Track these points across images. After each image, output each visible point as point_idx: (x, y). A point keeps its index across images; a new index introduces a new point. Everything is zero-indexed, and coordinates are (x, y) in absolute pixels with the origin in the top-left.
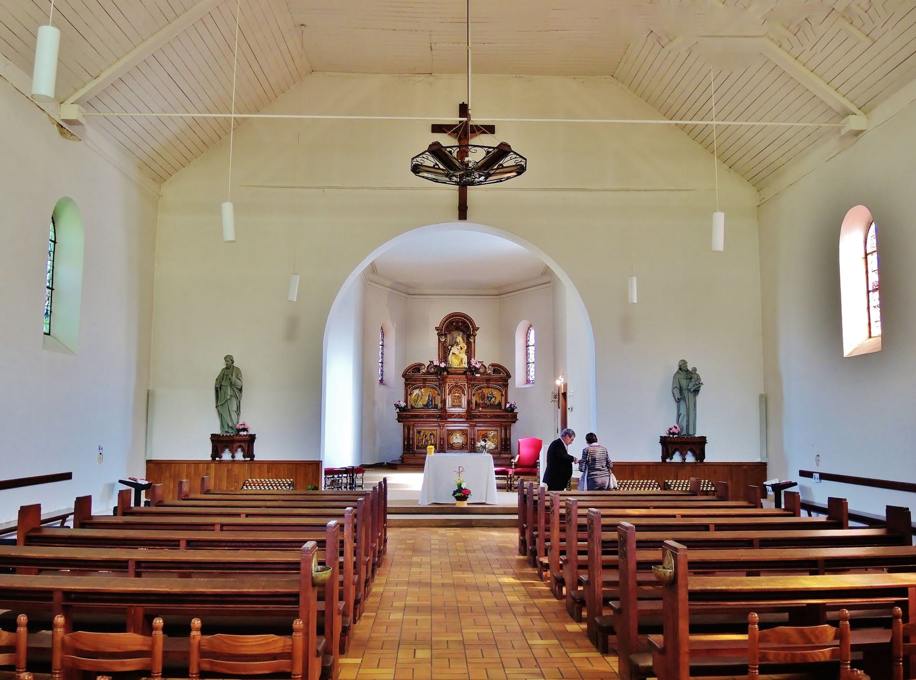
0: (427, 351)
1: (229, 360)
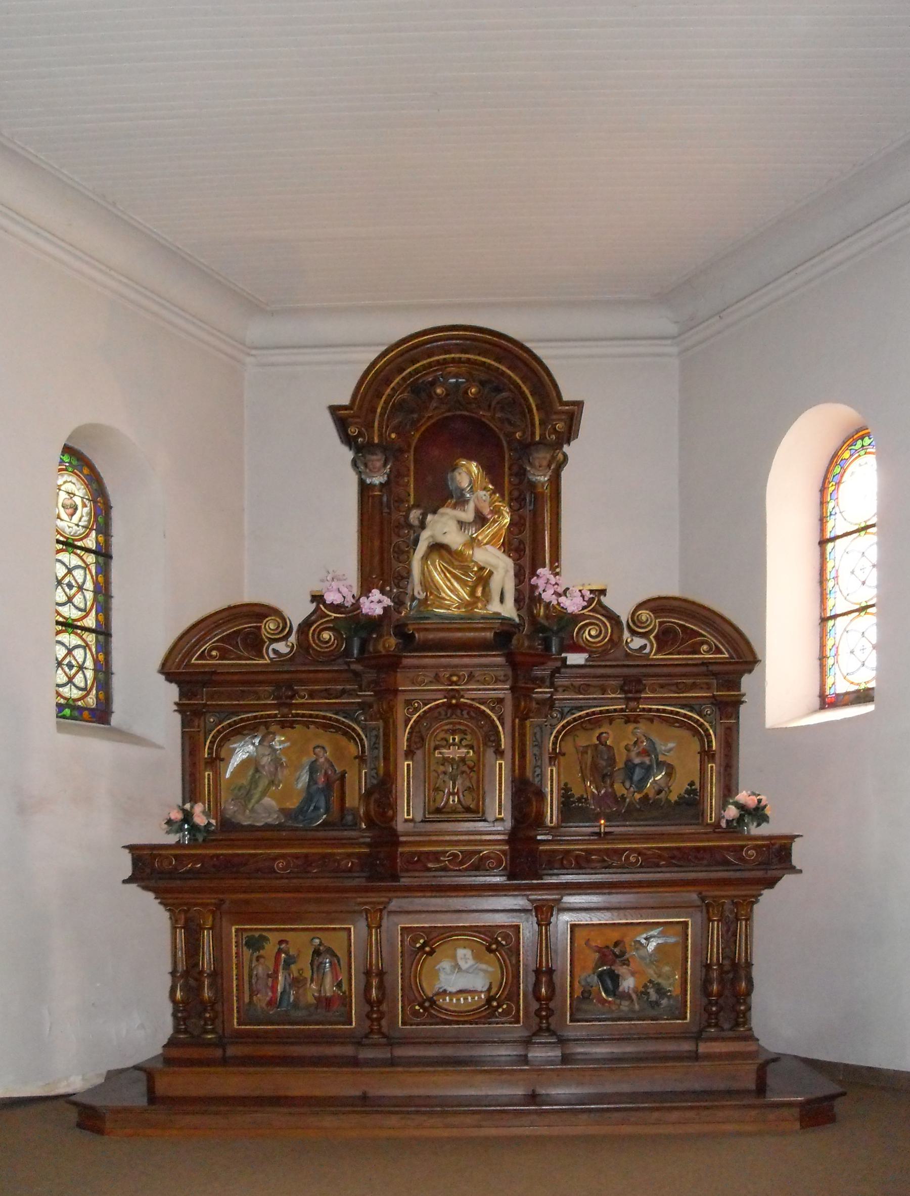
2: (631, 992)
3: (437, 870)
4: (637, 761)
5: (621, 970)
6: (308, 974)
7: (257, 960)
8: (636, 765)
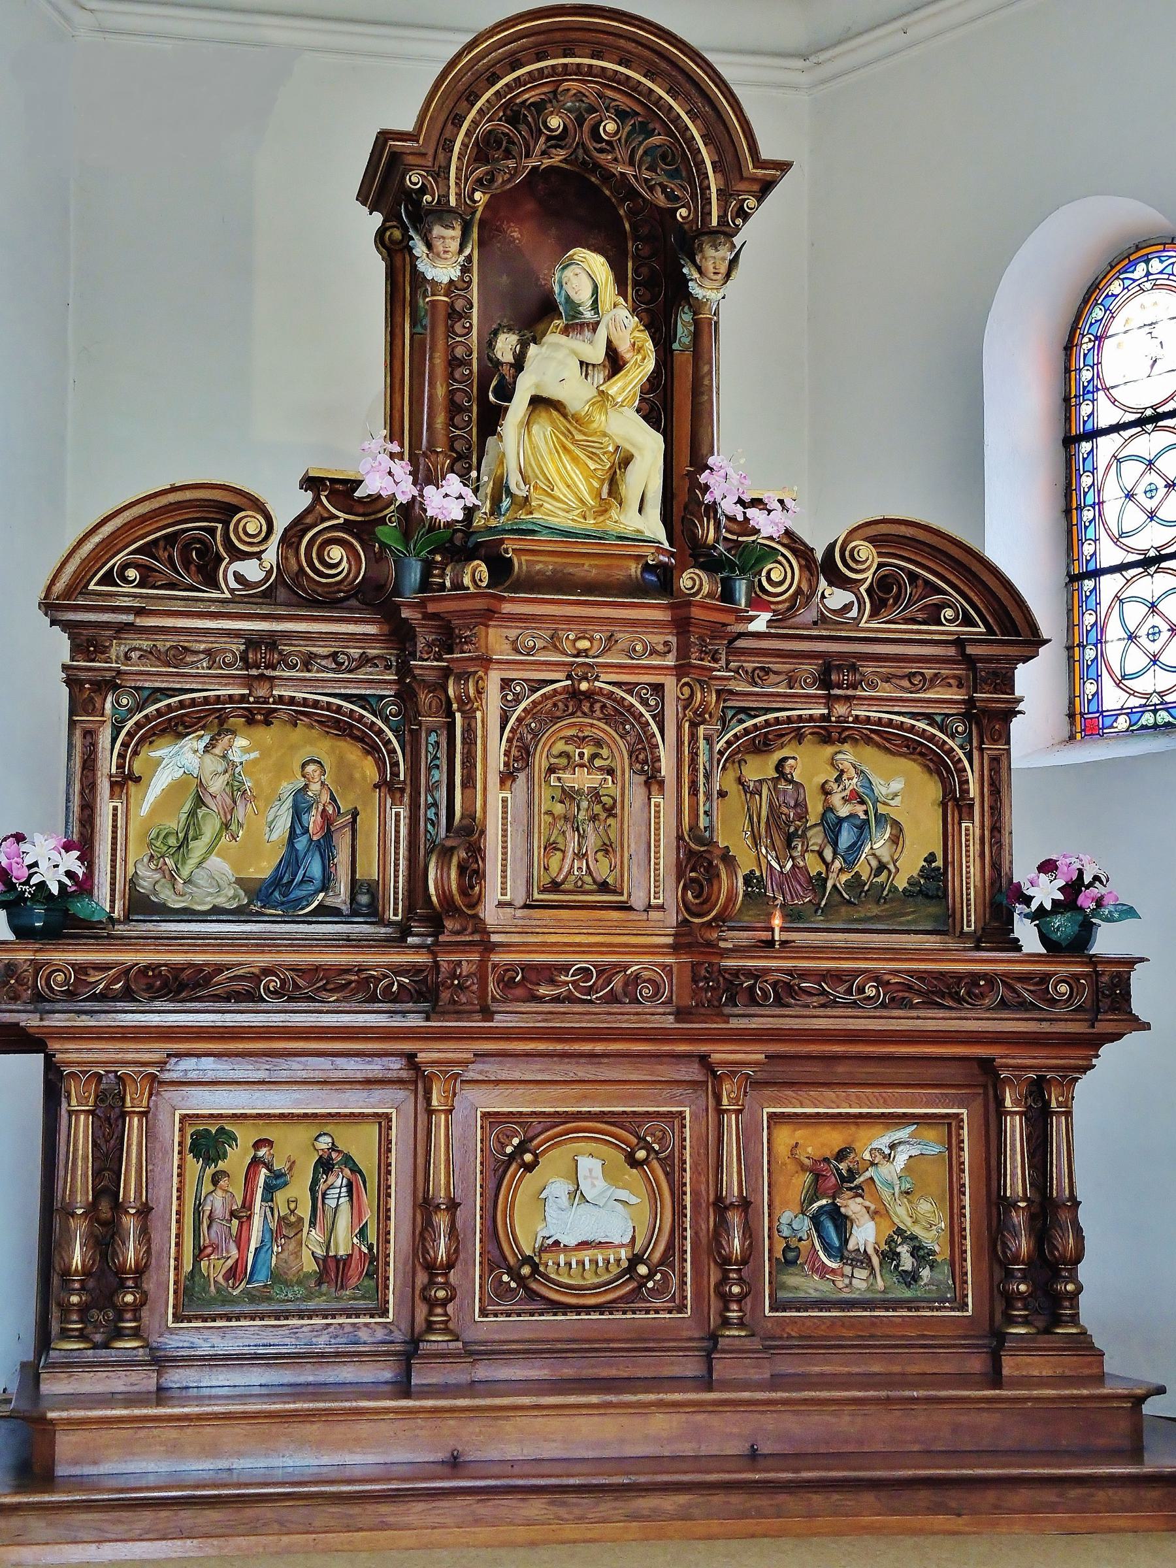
0: (298, 403)
1: (1146, 1026)
2: (870, 1251)
3: (556, 999)
4: (843, 811)
5: (852, 1207)
7: (215, 1181)
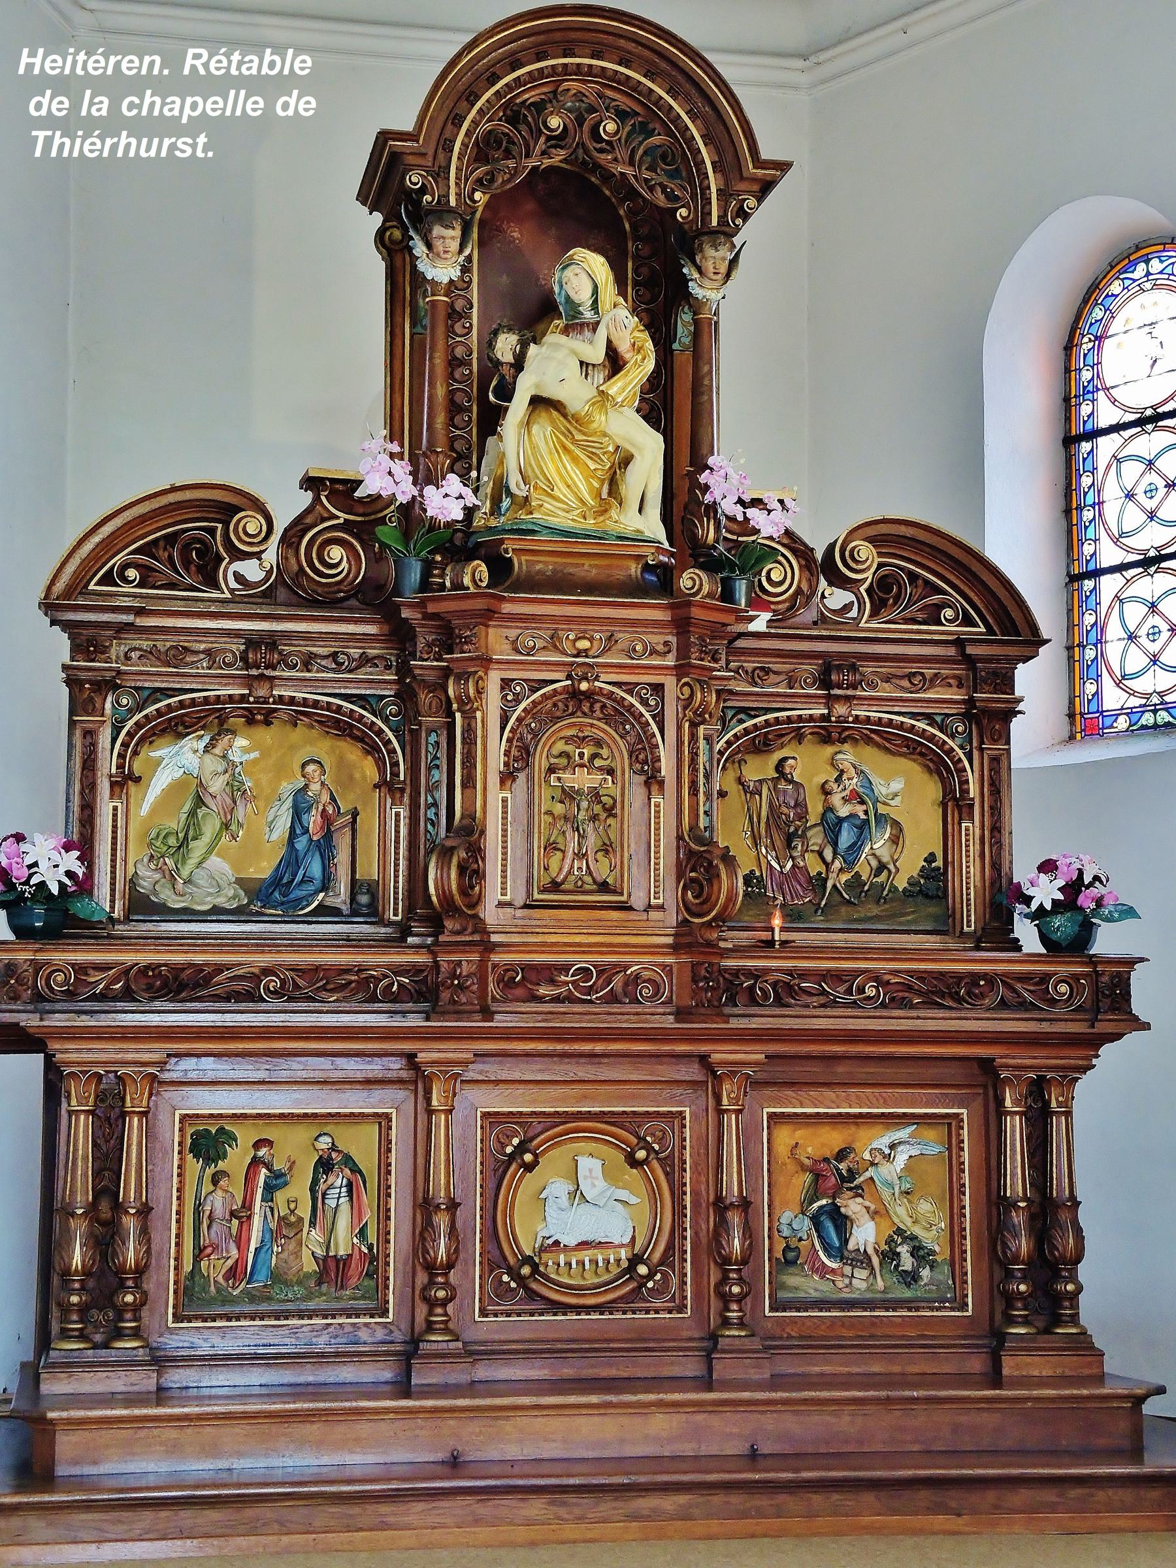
2: (870, 1251)
3: (556, 999)
4: (843, 811)
5: (852, 1207)
6: (305, 1212)
7: (215, 1181)
8: (841, 820)
